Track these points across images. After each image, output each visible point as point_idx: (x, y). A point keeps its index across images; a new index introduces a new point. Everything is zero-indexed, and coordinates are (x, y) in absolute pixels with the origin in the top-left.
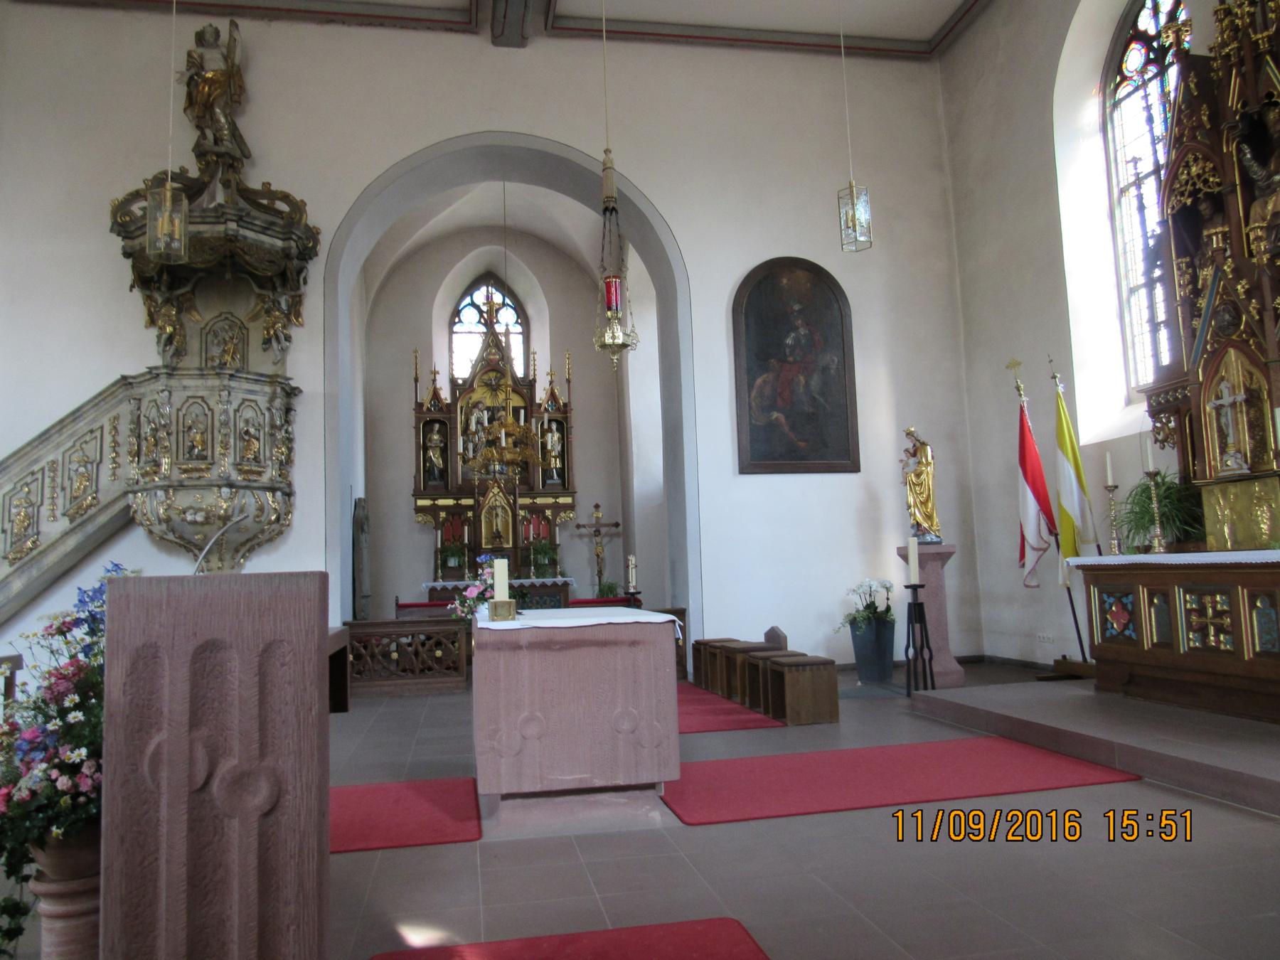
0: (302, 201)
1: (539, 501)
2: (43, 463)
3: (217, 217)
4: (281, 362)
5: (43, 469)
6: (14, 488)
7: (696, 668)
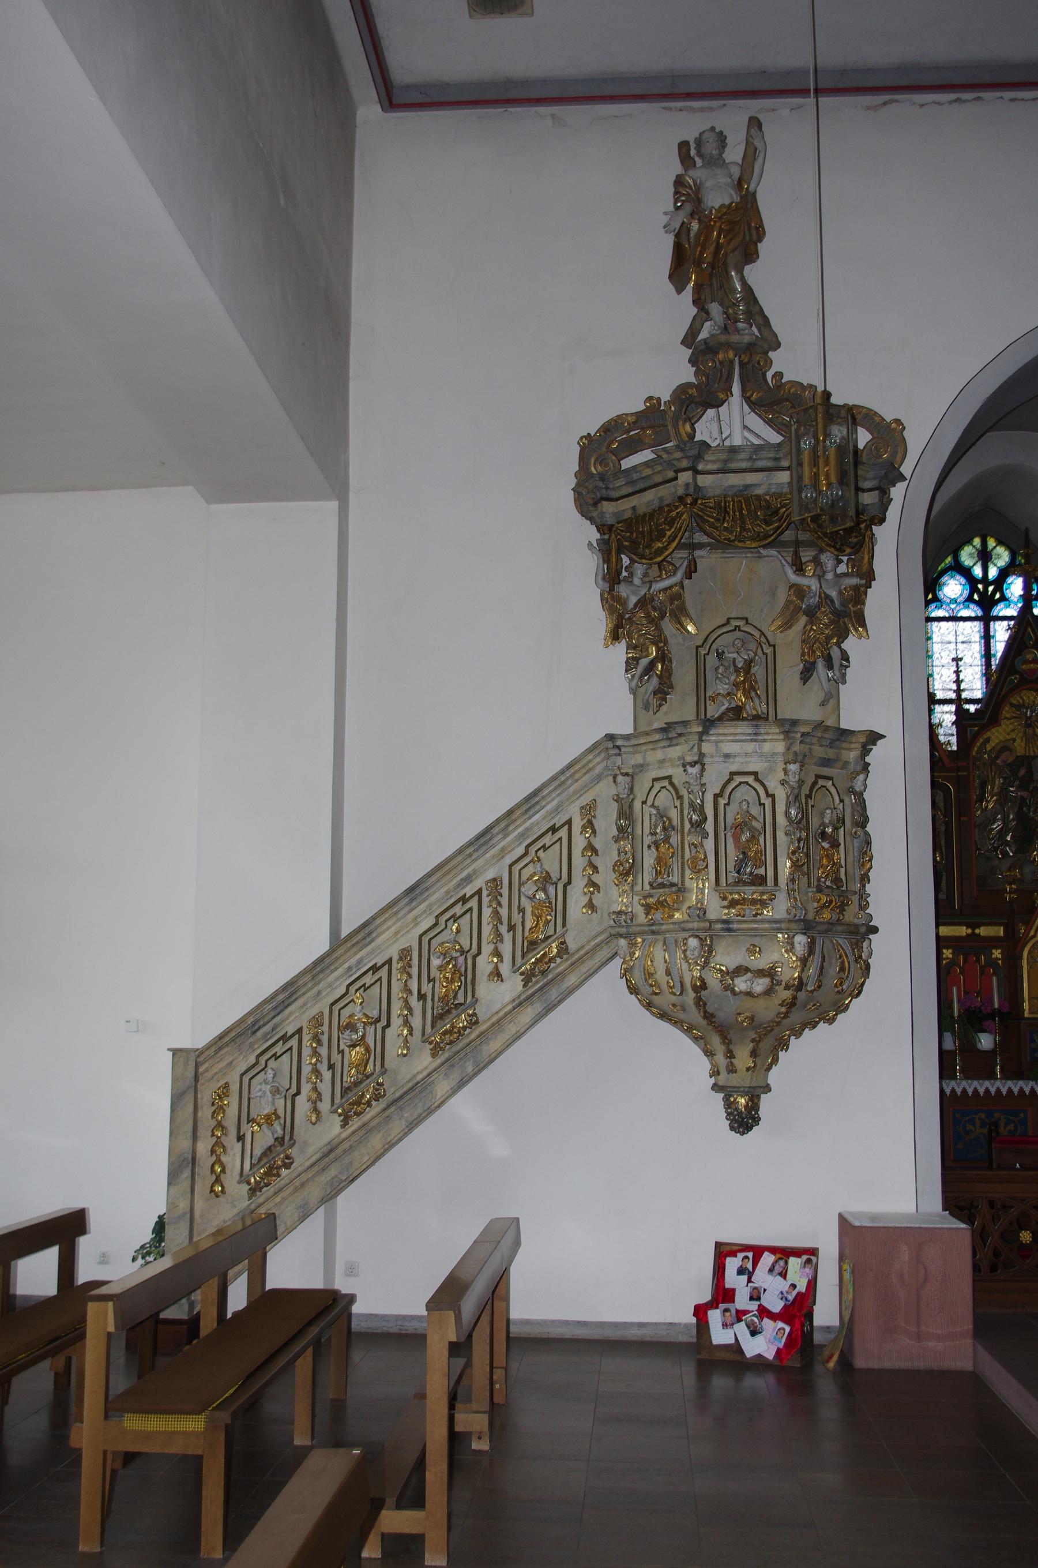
0: (898, 422)
2: (478, 883)
3: (776, 459)
4: (831, 699)
5: (479, 892)
6: (436, 924)
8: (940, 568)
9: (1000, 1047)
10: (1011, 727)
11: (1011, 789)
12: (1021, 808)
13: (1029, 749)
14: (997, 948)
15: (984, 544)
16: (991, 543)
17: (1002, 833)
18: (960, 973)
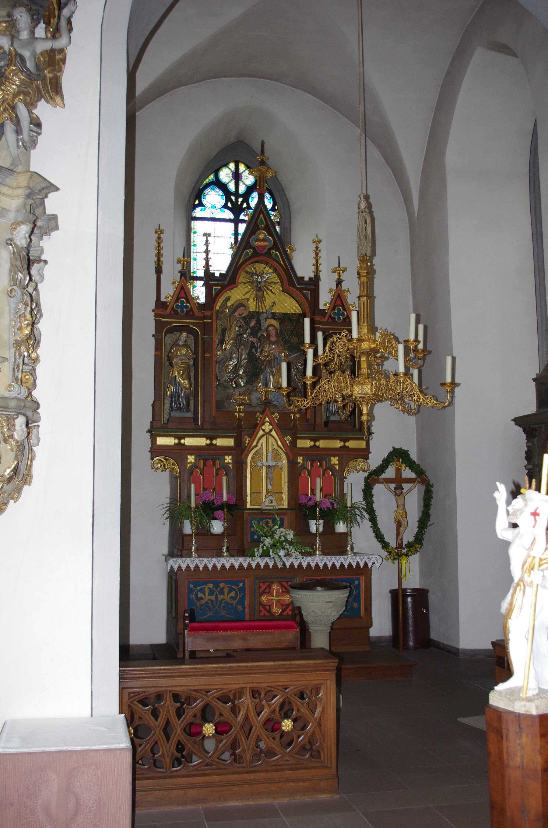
1: (321, 444)
7: (283, 660)
8: (205, 183)
9: (228, 532)
10: (247, 290)
11: (245, 336)
12: (251, 350)
13: (259, 306)
14: (228, 455)
15: (237, 168)
16: (242, 167)
17: (236, 368)
18: (201, 474)
